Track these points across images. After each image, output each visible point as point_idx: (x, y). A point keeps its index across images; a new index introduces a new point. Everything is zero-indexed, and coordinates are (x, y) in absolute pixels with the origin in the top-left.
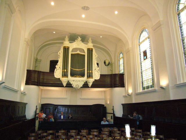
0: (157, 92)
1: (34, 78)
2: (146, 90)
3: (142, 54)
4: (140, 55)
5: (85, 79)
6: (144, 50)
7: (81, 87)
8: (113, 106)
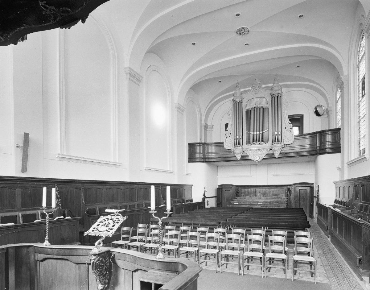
1: (196, 153)
8: (318, 186)
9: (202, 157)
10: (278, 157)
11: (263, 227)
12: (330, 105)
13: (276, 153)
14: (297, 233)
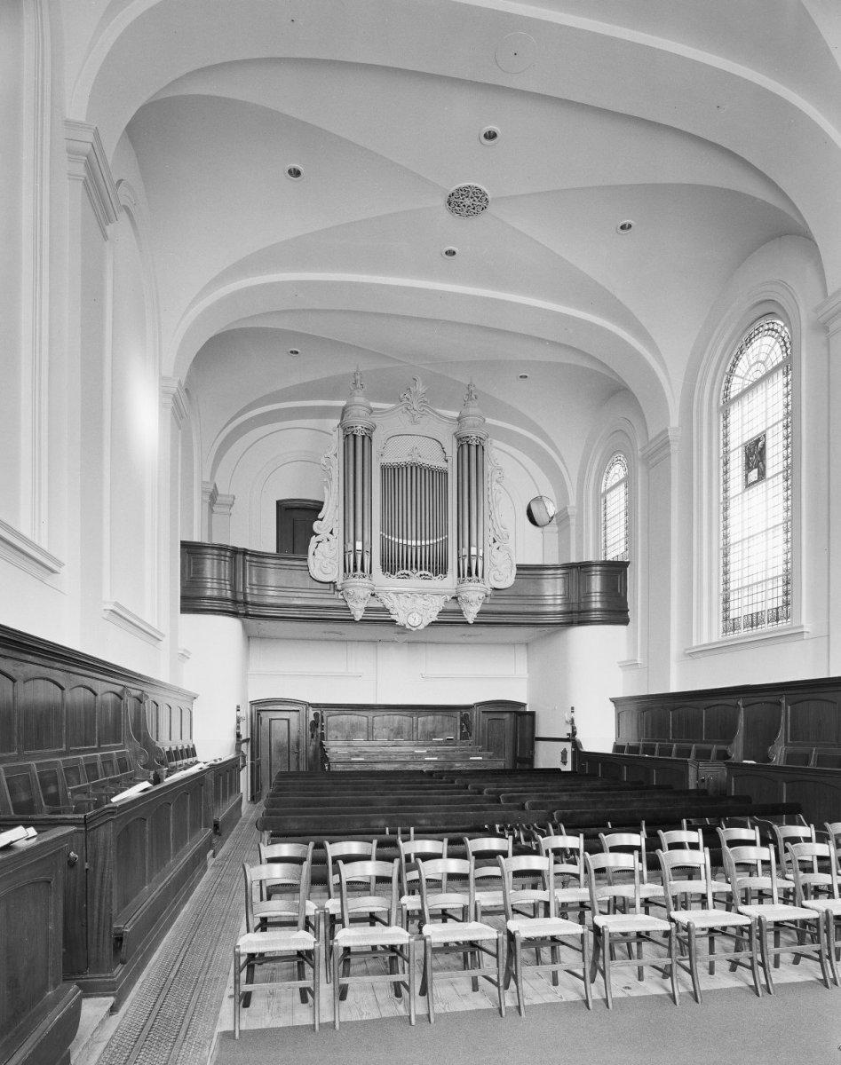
0: (805, 636)
1: (213, 580)
2: (742, 632)
3: (737, 461)
4: (726, 464)
5: (449, 582)
6: (750, 435)
7: (434, 624)
8: (573, 708)
9: (229, 594)
10: (474, 623)
11: (412, 829)
12: (573, 502)
13: (472, 609)
14: (667, 837)
